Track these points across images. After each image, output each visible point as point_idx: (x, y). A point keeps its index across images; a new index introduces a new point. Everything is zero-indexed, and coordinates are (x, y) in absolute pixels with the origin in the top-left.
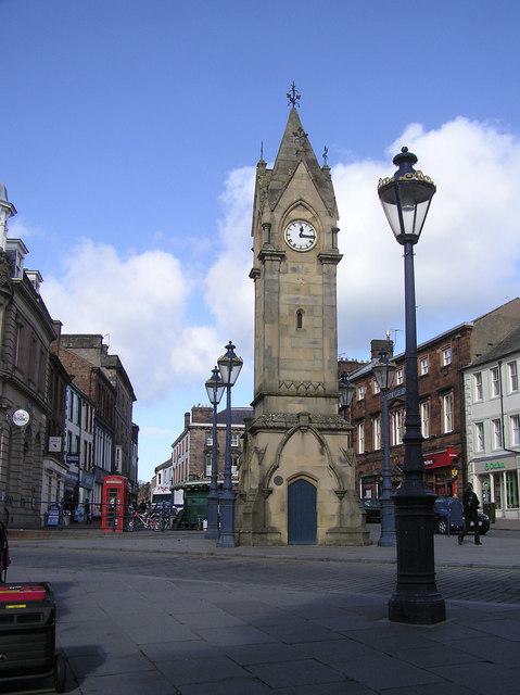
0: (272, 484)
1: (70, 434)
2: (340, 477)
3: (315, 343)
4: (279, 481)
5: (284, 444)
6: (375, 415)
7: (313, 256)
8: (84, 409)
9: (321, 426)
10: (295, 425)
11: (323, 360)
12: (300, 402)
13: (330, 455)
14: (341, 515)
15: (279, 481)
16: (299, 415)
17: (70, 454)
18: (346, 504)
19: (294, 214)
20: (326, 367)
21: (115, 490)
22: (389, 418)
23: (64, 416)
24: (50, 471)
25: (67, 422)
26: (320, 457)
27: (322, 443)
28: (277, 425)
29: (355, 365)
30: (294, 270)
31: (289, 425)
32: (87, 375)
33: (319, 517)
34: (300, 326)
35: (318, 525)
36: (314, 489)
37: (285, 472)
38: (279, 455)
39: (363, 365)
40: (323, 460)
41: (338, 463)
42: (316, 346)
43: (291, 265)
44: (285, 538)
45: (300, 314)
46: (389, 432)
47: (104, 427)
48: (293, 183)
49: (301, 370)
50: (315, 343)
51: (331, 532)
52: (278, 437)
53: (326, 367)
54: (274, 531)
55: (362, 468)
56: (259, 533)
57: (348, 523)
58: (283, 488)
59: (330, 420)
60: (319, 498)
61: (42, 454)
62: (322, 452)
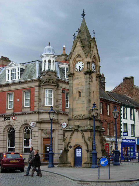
0: (69, 148)
4: (71, 147)
5: (72, 135)
7: (82, 73)
9: (82, 129)
12: (78, 122)
15: (71, 147)
30: (77, 78)
37: (73, 144)
38: (70, 139)
42: (83, 103)
44: (72, 165)
45: (80, 93)
50: (83, 102)
51: (85, 163)
52: (70, 133)
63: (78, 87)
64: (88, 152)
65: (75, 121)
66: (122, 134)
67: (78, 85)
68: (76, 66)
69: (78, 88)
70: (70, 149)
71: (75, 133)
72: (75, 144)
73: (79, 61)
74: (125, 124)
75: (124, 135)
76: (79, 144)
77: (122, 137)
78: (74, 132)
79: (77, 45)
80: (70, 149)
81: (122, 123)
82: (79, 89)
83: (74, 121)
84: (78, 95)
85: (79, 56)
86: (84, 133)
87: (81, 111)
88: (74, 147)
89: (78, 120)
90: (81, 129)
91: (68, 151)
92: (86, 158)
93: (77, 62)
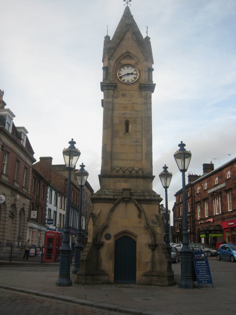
0: (103, 240)
1: (50, 210)
2: (153, 234)
3: (137, 142)
4: (108, 237)
5: (112, 210)
6: (205, 199)
7: (136, 86)
8: (59, 198)
9: (138, 198)
10: (120, 197)
11: (142, 153)
12: (126, 182)
13: (146, 218)
14: (153, 262)
15: (108, 237)
16: (124, 190)
17: (49, 220)
18: (157, 254)
19: (124, 62)
20: (144, 158)
21: (51, 239)
22: (212, 201)
23: (46, 201)
24: (31, 228)
25: (48, 204)
26: (139, 220)
27: (139, 209)
28: (107, 197)
29: (196, 177)
30: (123, 95)
31: (116, 197)
32: (63, 182)
33: (137, 263)
34: (127, 130)
35: (137, 269)
36: (135, 243)
37: (113, 230)
38: (109, 218)
39: (200, 176)
40: (140, 222)
41: (151, 224)
42: (138, 144)
43: (121, 92)
44: (112, 279)
45: (127, 124)
46: (212, 208)
47: (73, 207)
48: (123, 43)
49: (127, 160)
50: (137, 142)
51: (145, 275)
52: (109, 206)
53: (144, 158)
54: (104, 273)
55: (39, 222)
56: (91, 275)
57: (158, 268)
58: (111, 242)
59: (146, 194)
60: (138, 250)
61: (26, 219)
62: (140, 216)
63: (125, 112)
64: (153, 250)
65: (118, 179)
66: (46, 221)
67: (125, 108)
68: (122, 69)
69: (125, 114)
70: (107, 242)
71: (121, 207)
72: (121, 230)
73: (128, 65)
74: (64, 210)
75: (48, 224)
76: (131, 230)
77: (46, 225)
78: (117, 204)
79: (126, 37)
80: (107, 242)
81: (47, 208)
82: (128, 116)
83: (116, 179)
84: (122, 128)
85: (128, 55)
86: (145, 207)
87: (131, 160)
88: (116, 236)
89: (124, 179)
90: (136, 197)
91: (102, 245)
92: (148, 263)
93: (123, 66)
